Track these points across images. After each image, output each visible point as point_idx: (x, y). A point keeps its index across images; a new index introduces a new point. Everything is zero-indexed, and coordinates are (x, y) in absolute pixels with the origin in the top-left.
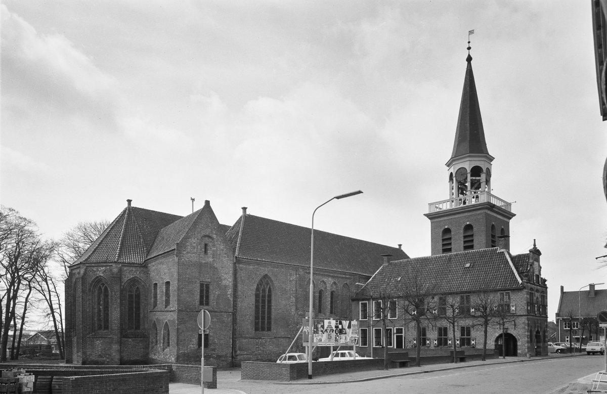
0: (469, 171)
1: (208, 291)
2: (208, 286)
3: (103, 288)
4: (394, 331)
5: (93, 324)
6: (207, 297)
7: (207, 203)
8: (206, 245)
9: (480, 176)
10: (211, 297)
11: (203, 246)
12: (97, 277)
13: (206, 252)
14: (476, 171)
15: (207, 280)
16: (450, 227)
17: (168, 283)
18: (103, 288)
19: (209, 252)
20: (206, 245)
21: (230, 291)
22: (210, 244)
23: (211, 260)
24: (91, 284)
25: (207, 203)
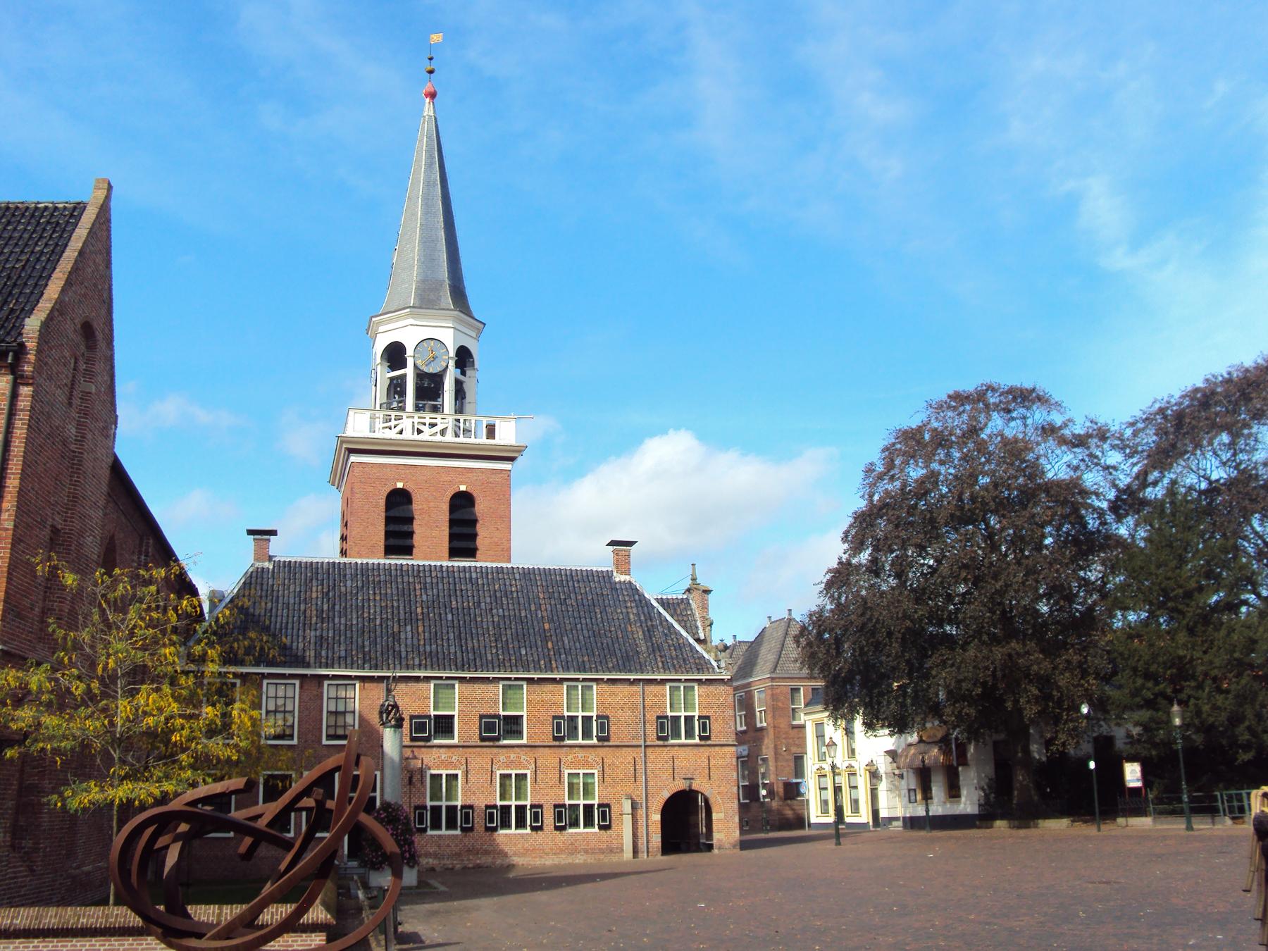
0: (452, 353)
16: (410, 487)
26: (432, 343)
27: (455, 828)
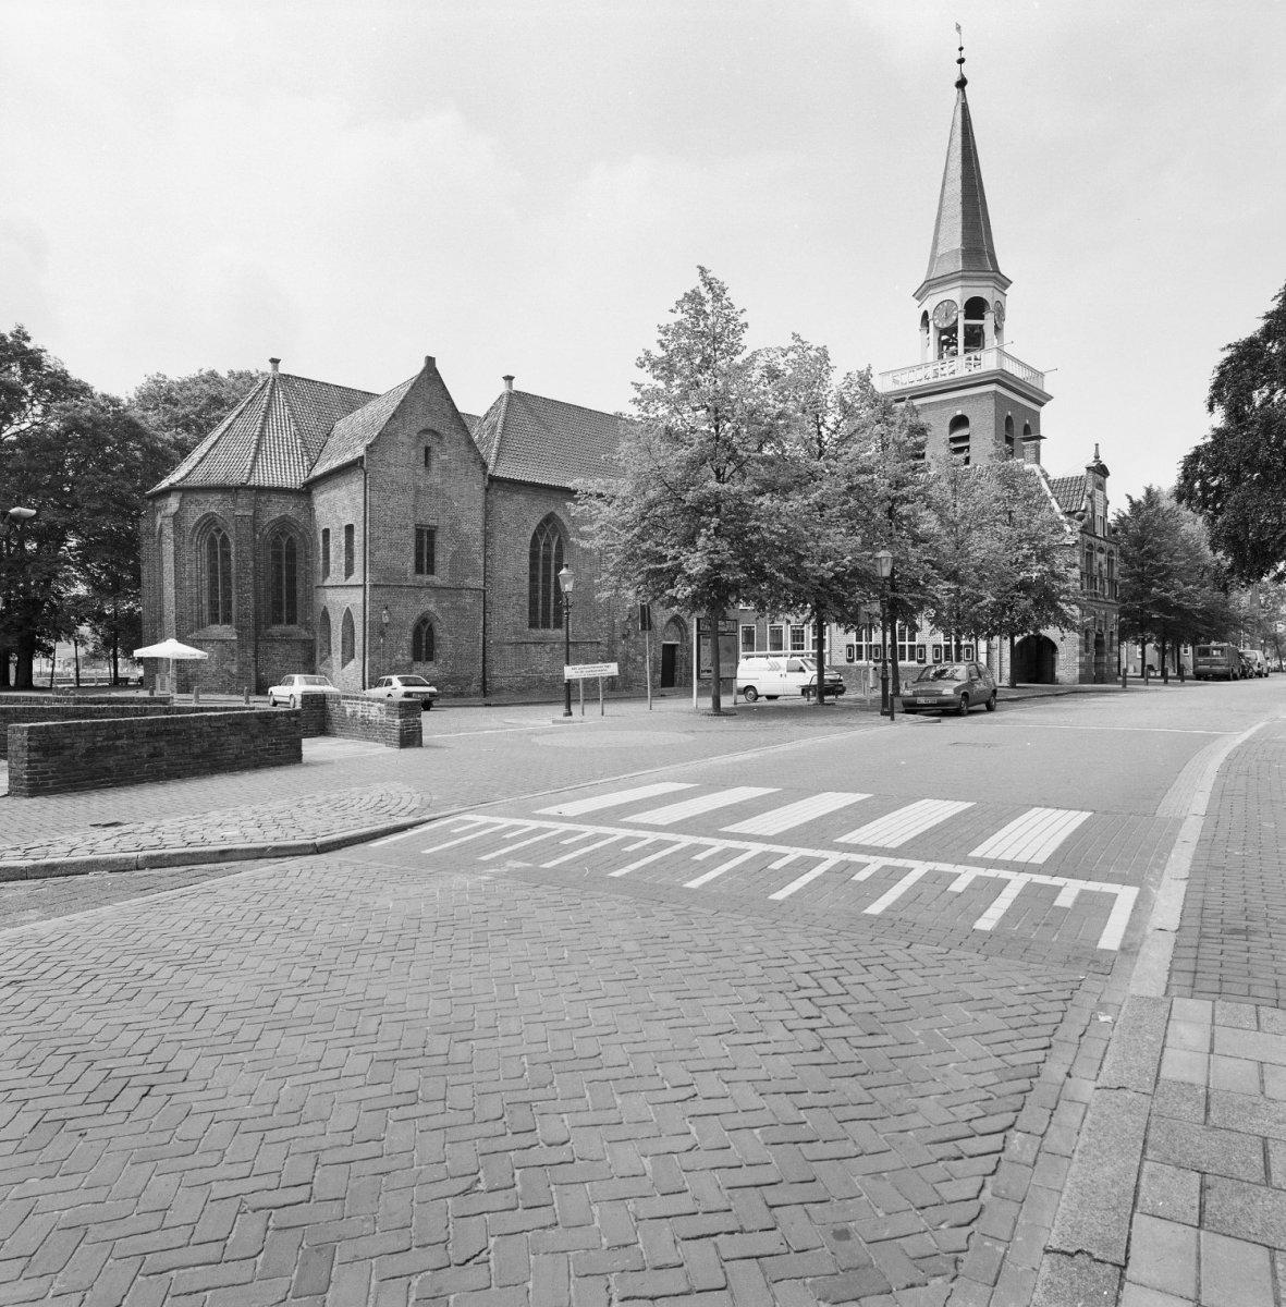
0: (961, 307)
1: (432, 545)
2: (432, 533)
3: (219, 539)
4: (787, 635)
5: (200, 613)
6: (431, 557)
7: (430, 361)
8: (427, 450)
9: (982, 318)
10: (439, 558)
11: (423, 452)
12: (207, 515)
13: (427, 463)
14: (975, 307)
15: (431, 522)
17: (350, 529)
18: (219, 539)
19: (434, 464)
20: (427, 450)
21: (478, 546)
22: (437, 448)
23: (438, 480)
24: (195, 529)
25: (430, 361)
26: (946, 304)
27: (914, 659)
